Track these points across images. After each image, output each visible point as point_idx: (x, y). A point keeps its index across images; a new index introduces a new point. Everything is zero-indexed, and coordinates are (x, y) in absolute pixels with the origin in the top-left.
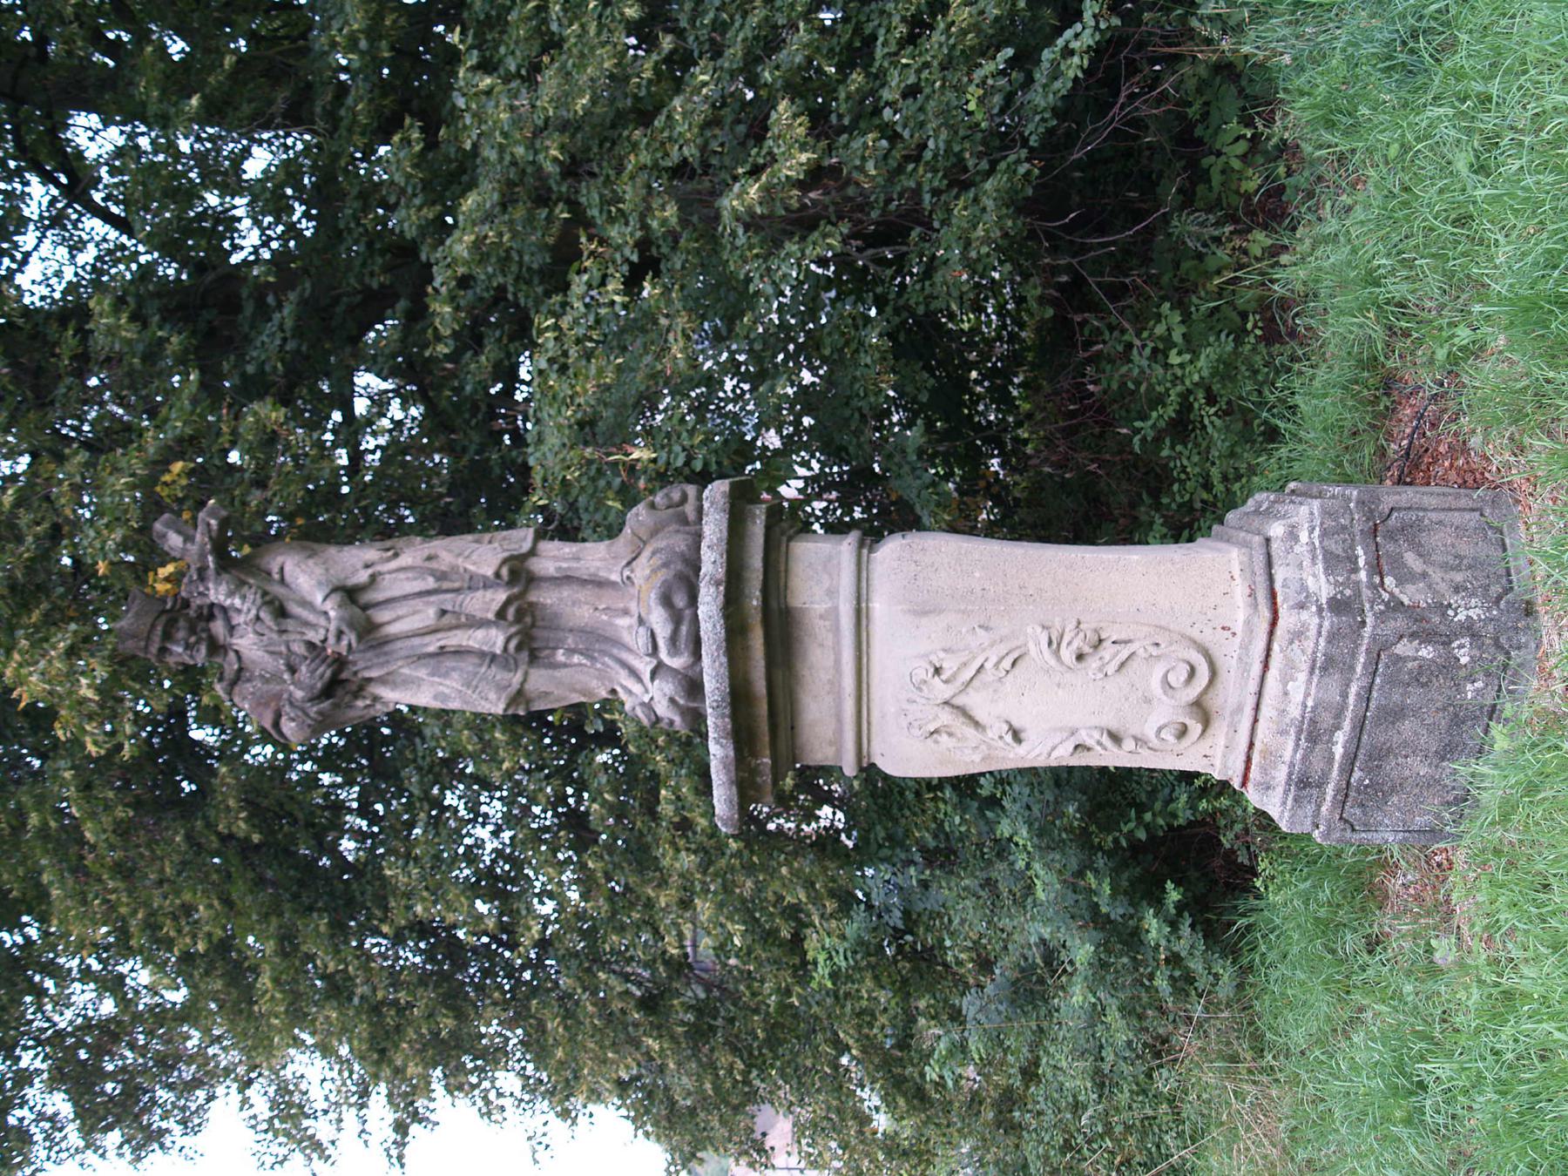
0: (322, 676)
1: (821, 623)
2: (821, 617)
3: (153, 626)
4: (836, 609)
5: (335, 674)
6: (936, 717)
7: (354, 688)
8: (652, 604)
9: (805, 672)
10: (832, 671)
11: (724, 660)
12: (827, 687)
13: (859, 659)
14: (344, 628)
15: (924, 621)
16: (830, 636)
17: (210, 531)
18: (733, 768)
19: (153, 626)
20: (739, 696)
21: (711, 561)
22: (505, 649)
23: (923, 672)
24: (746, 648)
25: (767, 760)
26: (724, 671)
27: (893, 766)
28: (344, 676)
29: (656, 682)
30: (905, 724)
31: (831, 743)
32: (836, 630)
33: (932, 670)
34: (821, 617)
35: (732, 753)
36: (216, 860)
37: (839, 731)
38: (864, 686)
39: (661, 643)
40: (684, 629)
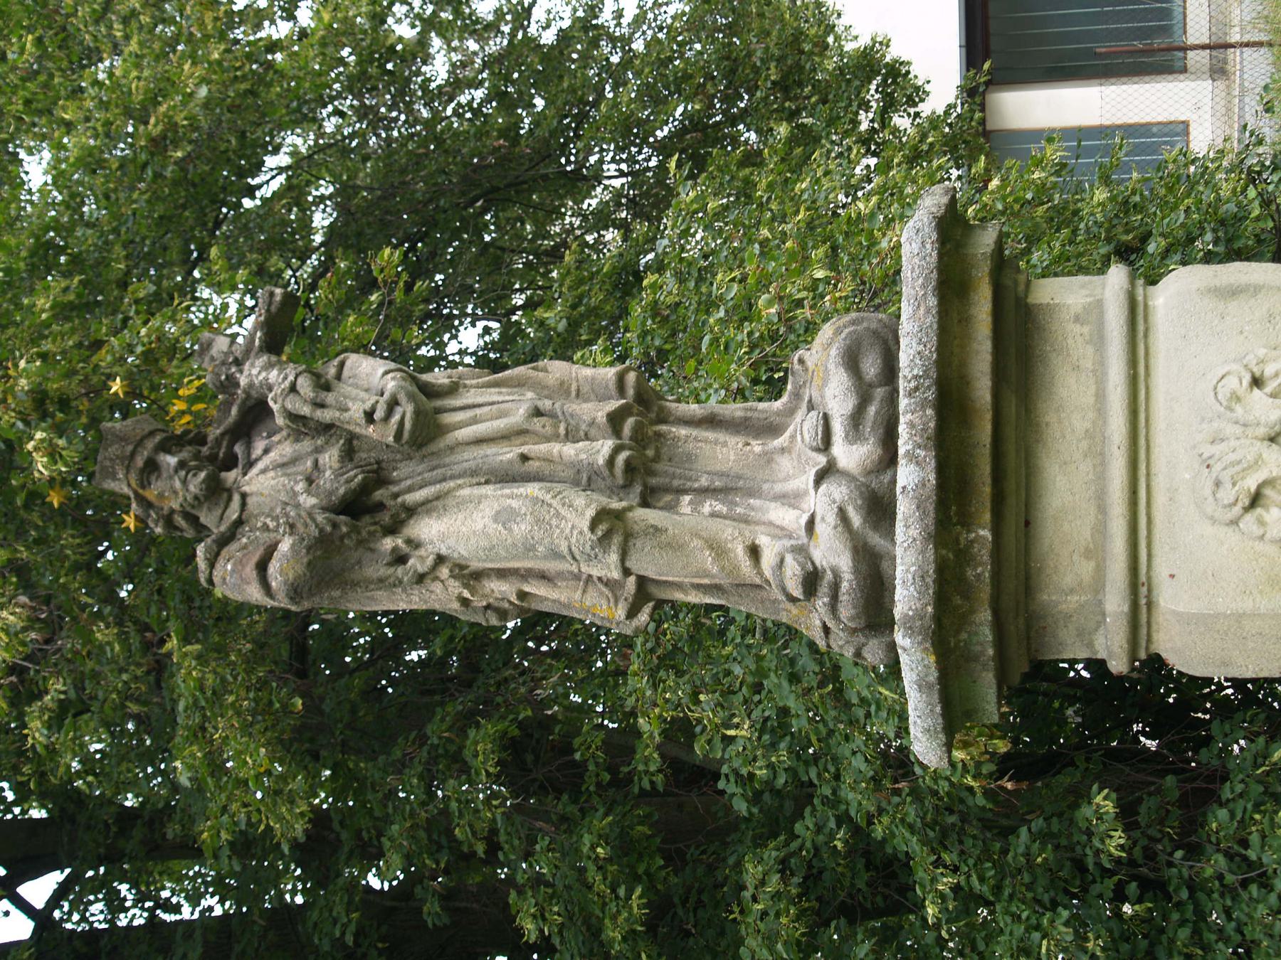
0: (348, 481)
1: (1077, 329)
2: (1077, 319)
3: (152, 433)
4: (1099, 305)
5: (366, 489)
6: (1257, 463)
7: (386, 518)
8: (831, 366)
9: (1051, 417)
10: (1091, 415)
11: (932, 301)
12: (1084, 445)
13: (1133, 362)
14: (402, 398)
15: (1233, 306)
16: (1090, 350)
17: (270, 304)
18: (931, 508)
19: (152, 433)
20: (948, 582)
21: (913, 353)
22: (611, 462)
23: (1237, 383)
24: (966, 321)
25: (985, 533)
26: (931, 320)
27: (1186, 652)
28: (379, 495)
29: (823, 488)
30: (1209, 484)
31: (1088, 554)
32: (1099, 340)
33: (1247, 379)
34: (1077, 319)
35: (932, 477)
36: (152, 272)
37: (1101, 529)
38: (1142, 442)
39: (838, 428)
40: (872, 410)
